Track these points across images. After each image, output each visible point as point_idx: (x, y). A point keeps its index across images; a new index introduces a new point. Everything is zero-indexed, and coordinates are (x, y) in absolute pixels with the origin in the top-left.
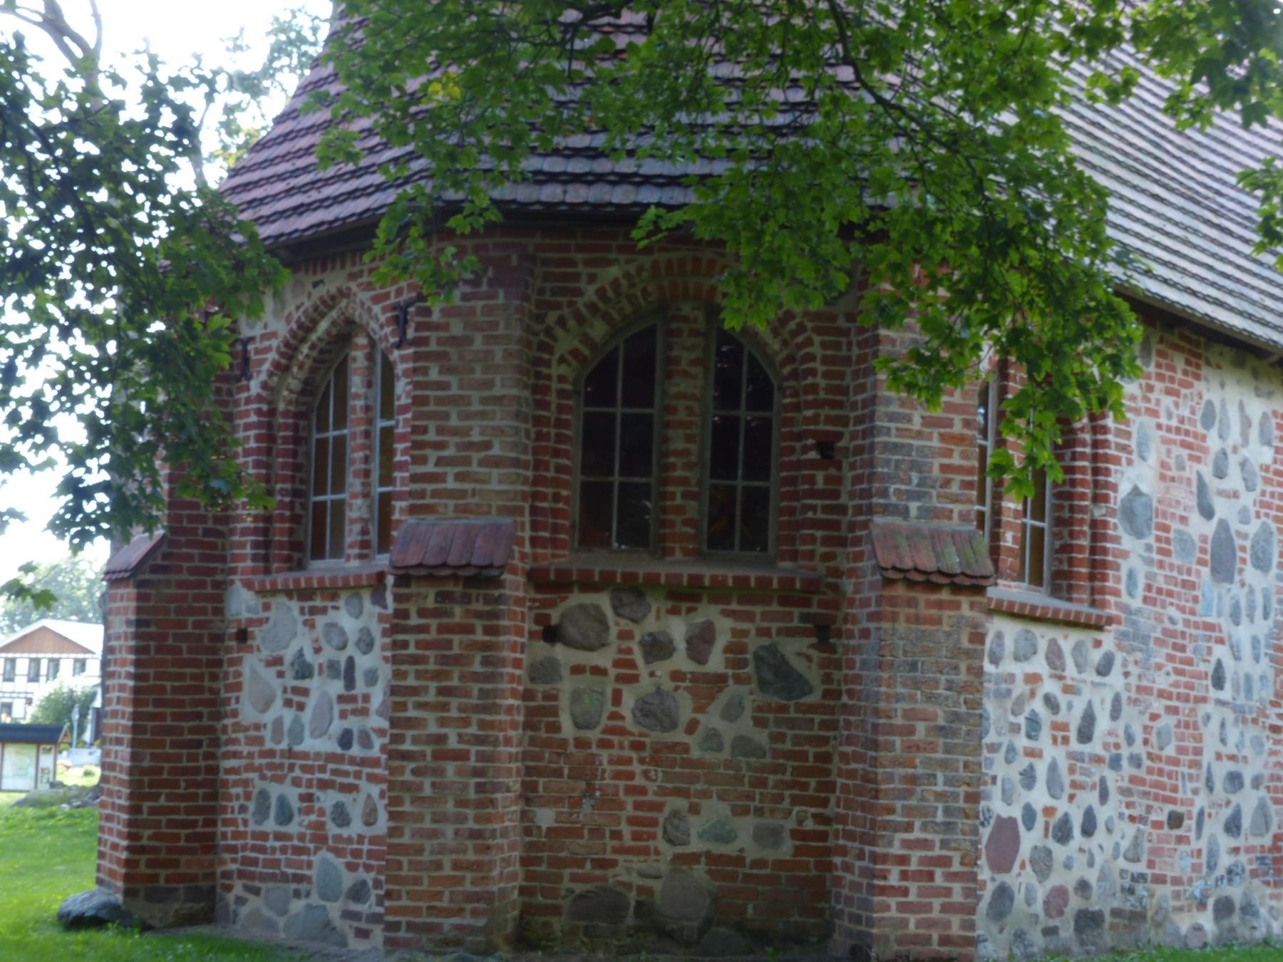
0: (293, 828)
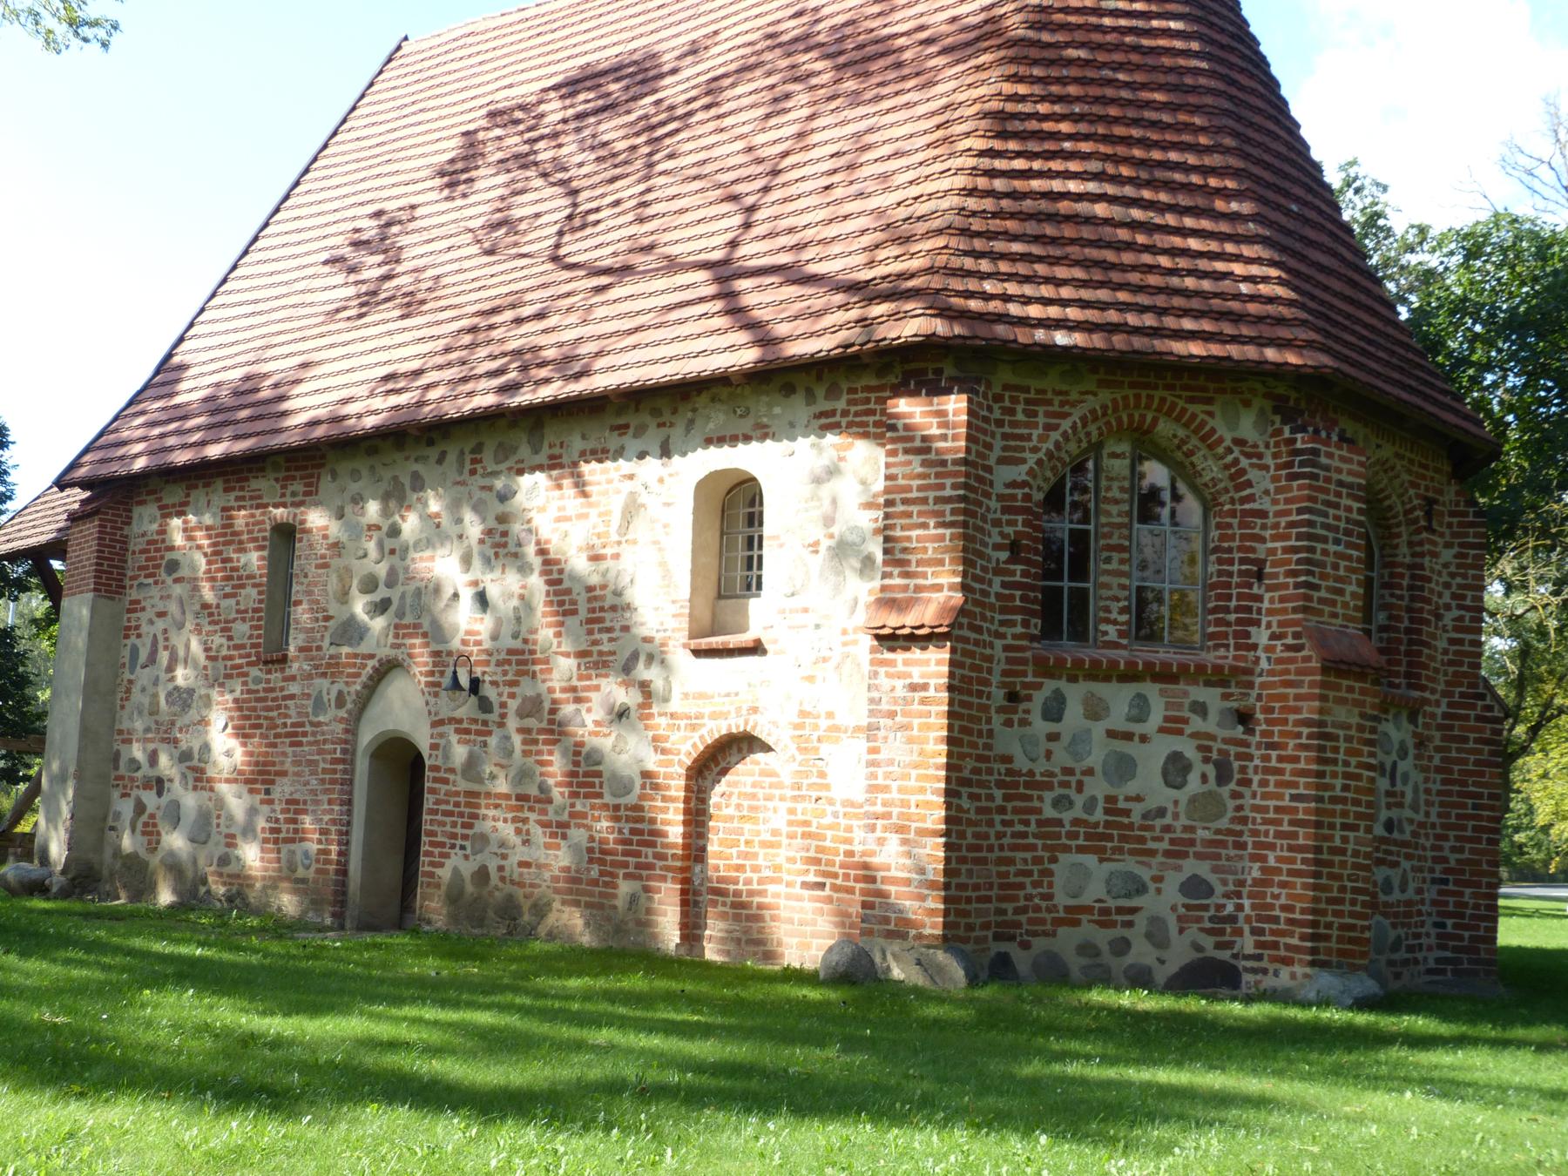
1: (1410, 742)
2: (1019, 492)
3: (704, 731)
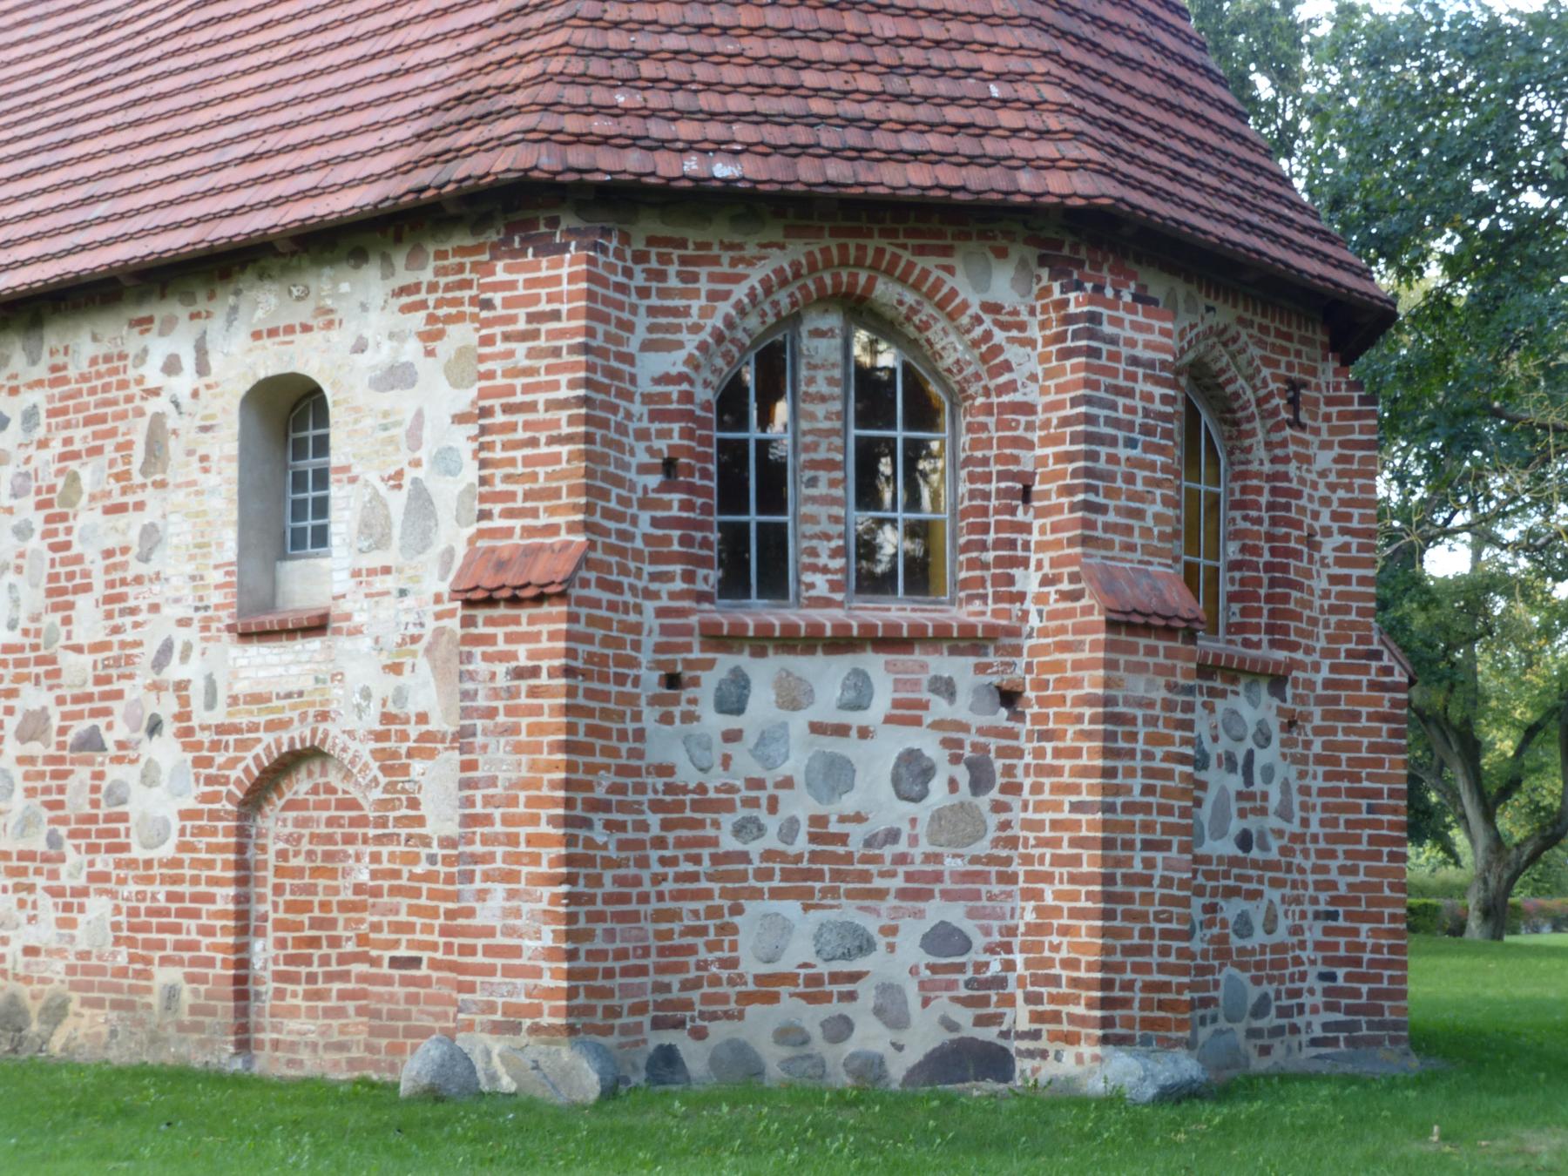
1: (1274, 724)
2: (674, 390)
3: (259, 749)
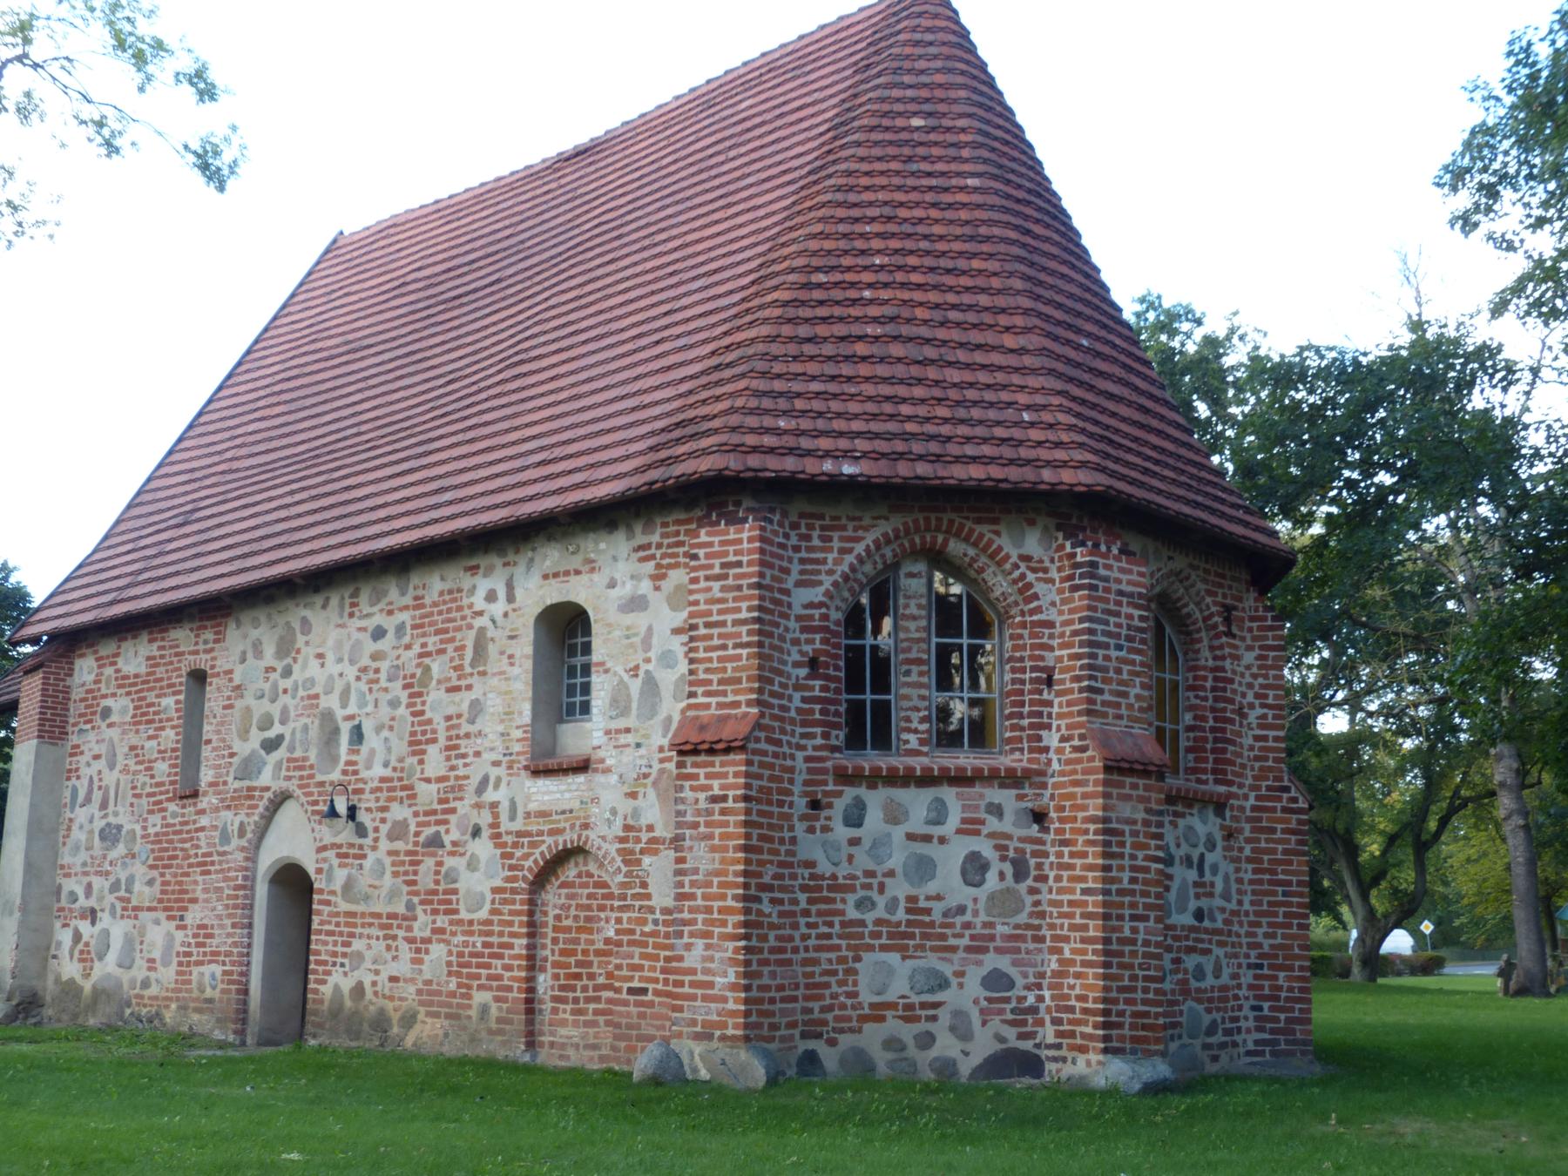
0: (1167, 986)
2: (816, 613)
3: (544, 848)
